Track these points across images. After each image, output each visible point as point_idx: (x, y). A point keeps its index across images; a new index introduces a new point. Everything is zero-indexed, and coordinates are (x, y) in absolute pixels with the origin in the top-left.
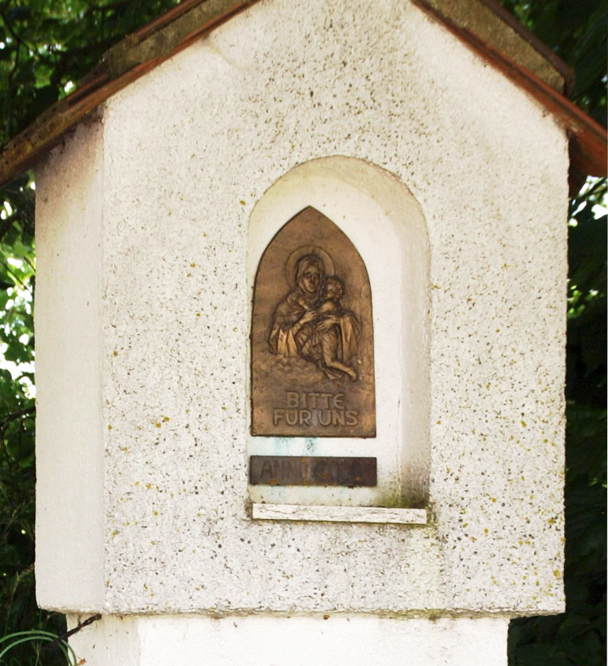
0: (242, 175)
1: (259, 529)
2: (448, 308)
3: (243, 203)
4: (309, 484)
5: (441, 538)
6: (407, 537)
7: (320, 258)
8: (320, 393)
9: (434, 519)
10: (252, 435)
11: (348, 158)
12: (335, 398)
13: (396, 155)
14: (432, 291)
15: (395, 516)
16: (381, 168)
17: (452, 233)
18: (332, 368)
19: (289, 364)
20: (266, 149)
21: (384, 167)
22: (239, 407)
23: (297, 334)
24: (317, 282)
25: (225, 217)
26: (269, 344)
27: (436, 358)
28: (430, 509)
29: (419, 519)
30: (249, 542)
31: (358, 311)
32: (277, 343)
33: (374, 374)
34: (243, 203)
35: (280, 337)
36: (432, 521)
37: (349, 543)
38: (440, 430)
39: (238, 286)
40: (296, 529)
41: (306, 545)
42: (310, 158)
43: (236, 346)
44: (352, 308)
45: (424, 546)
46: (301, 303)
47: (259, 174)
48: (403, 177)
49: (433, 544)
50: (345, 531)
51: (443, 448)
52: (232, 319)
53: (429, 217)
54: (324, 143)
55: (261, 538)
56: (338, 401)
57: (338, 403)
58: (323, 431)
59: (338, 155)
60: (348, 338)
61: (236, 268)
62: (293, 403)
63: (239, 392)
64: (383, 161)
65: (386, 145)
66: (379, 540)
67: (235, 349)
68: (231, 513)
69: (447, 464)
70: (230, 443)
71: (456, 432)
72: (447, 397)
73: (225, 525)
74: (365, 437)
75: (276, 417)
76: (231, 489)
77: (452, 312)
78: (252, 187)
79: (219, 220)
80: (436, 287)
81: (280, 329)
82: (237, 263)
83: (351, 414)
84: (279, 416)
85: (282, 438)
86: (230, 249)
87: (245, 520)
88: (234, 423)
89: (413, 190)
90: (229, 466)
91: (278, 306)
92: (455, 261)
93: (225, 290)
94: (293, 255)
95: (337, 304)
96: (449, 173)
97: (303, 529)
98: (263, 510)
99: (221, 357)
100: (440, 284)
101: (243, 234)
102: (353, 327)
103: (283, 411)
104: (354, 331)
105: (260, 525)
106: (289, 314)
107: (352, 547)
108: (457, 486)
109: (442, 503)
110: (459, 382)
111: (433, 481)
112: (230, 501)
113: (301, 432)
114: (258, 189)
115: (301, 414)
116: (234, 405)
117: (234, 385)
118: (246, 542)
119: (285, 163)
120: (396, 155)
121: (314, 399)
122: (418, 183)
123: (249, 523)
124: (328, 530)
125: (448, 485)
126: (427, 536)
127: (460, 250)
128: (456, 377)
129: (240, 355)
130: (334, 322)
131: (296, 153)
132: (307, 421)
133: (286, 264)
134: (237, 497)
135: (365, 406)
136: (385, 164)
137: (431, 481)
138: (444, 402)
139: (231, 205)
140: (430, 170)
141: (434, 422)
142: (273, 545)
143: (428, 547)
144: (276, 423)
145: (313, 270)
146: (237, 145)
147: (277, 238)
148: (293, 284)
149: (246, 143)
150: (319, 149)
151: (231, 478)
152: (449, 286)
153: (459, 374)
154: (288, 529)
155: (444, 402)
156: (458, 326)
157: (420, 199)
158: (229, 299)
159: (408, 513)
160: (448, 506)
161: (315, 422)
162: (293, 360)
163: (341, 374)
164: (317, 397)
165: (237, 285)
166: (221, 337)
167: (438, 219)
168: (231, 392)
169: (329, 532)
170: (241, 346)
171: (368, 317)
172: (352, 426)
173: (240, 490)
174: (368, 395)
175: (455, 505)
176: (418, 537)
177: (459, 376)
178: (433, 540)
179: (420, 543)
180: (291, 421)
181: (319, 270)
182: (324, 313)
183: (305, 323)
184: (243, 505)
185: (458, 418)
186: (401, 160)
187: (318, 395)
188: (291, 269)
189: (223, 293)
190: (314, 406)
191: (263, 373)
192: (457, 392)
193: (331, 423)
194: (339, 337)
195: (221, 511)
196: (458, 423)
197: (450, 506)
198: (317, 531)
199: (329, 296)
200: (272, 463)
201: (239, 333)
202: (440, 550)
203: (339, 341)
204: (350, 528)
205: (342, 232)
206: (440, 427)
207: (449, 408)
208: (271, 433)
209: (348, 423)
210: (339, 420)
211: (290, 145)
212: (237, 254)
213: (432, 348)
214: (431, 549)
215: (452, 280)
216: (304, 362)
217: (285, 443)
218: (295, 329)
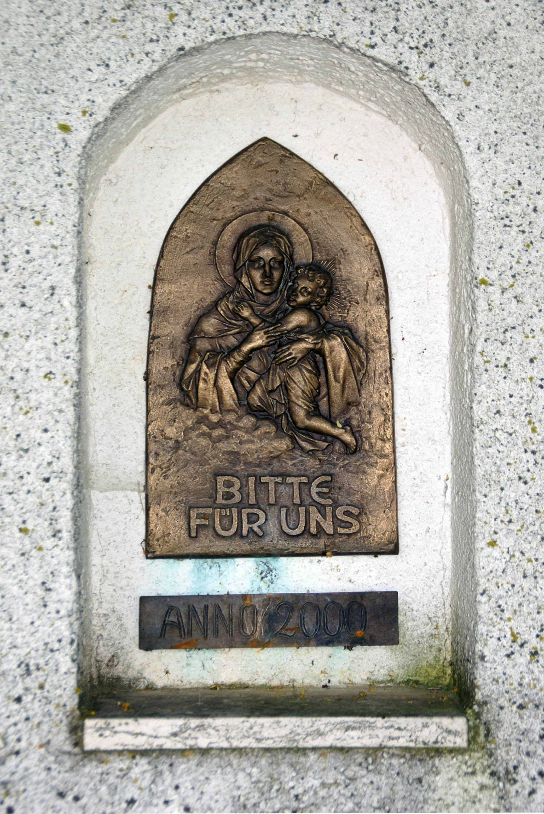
0: (62, 74)
1: (100, 770)
2: (511, 321)
3: (65, 128)
4: (261, 644)
5: (502, 773)
6: (426, 774)
7: (282, 232)
8: (284, 475)
9: (487, 736)
10: (147, 558)
11: (295, 36)
12: (314, 484)
13: (395, 29)
14: (476, 291)
15: (397, 733)
16: (364, 55)
17: (518, 177)
18: (310, 431)
19: (220, 424)
20: (114, 21)
21: (371, 52)
22: (58, 527)
23: (235, 371)
24: (276, 274)
25: (26, 157)
26: (182, 389)
27: (485, 418)
28: (478, 715)
29: (451, 738)
30: (76, 799)
31: (361, 327)
32: (197, 387)
33: (393, 440)
34: (65, 128)
35: (203, 375)
36: (481, 738)
37: (300, 791)
38: (496, 559)
39: (56, 292)
40: (183, 766)
41: (205, 797)
42: (212, 39)
43: (51, 407)
44: (350, 318)
45: (466, 791)
46: (246, 313)
47: (99, 72)
48: (411, 72)
49: (483, 787)
50: (292, 765)
51: (502, 592)
52: (42, 355)
53: (468, 149)
54: (240, 8)
55: (104, 789)
56: (320, 490)
57: (318, 493)
58: (291, 545)
59: (270, 32)
60: (341, 374)
61: (50, 256)
62: (229, 496)
63: (57, 497)
64: (368, 42)
65: (374, 10)
66: (365, 780)
67: (50, 413)
68: (36, 741)
69: (512, 623)
70: (37, 599)
71: (530, 560)
72: (511, 494)
73: (22, 766)
74: (376, 554)
75: (194, 524)
76: (38, 692)
77: (520, 329)
78: (84, 97)
79: (13, 162)
80: (484, 282)
81: (201, 362)
82: (54, 247)
83: (347, 513)
84: (198, 522)
85: (209, 561)
86: (38, 218)
87: (69, 753)
88: (48, 558)
89: (434, 97)
90: (33, 645)
91: (199, 319)
92: (523, 232)
93: (26, 299)
94: (229, 227)
95: (315, 314)
96: (510, 62)
97: (199, 764)
98: (107, 733)
99: (19, 429)
100: (493, 275)
101: (66, 188)
102: (349, 354)
103: (209, 511)
104: (351, 362)
105: (102, 762)
106: (222, 334)
107: (305, 798)
108: (534, 667)
109: (502, 701)
110: (536, 463)
111: (483, 658)
112: (35, 715)
113: (246, 547)
114: (99, 100)
115: (244, 517)
116: (47, 524)
117: (47, 485)
118: (70, 798)
119: (156, 49)
120: (395, 29)
121: (272, 486)
122: (443, 81)
123: (79, 757)
124: (253, 765)
125: (514, 666)
126: (470, 770)
127: (535, 210)
128: (529, 454)
129: (59, 426)
130: (310, 346)
131: (179, 30)
132: (256, 529)
133: (215, 243)
134: (51, 708)
135: (375, 498)
136: (373, 47)
137: (477, 660)
138: (503, 504)
139: (39, 133)
140: (471, 58)
141: (481, 543)
142: (131, 802)
143: (473, 793)
144: (193, 535)
145: (267, 253)
146: (49, 14)
147: (197, 197)
148: (230, 280)
149: (70, 10)
150: (228, 20)
151: (38, 669)
152: (511, 281)
153: (533, 447)
154: (164, 767)
155: (503, 504)
156: (532, 356)
157: (449, 114)
158: (37, 316)
159: (425, 726)
160: (514, 708)
161: (272, 528)
162: (230, 417)
163: (325, 441)
164: (276, 483)
165: (53, 288)
166: (20, 391)
167: (487, 153)
168: (40, 497)
169: (255, 770)
170: (63, 406)
171: (382, 334)
172: (349, 535)
173: (59, 692)
174: (381, 476)
175: (530, 706)
176: (452, 773)
177: (534, 452)
178: (485, 779)
179: (455, 784)
180: (224, 529)
181: (281, 253)
182: (289, 332)
183: (253, 350)
184: (65, 722)
185: (535, 534)
186: (407, 39)
187: (279, 480)
188: (224, 253)
189: (23, 305)
190: (272, 501)
191: (171, 443)
192: (530, 483)
193: (307, 530)
194: (322, 373)
195: (15, 737)
196: (534, 544)
197: (521, 707)
198: (229, 769)
199: (301, 299)
200: (183, 610)
201: (58, 382)
202: (502, 798)
203: (322, 379)
204: (302, 759)
205: (329, 183)
206: (496, 552)
207: (514, 514)
208: (185, 552)
209: (341, 530)
210: (324, 526)
211: (165, 13)
212: (53, 228)
213: (476, 399)
214: (480, 796)
215: (518, 268)
216: (253, 420)
217: (215, 569)
218: (232, 364)
